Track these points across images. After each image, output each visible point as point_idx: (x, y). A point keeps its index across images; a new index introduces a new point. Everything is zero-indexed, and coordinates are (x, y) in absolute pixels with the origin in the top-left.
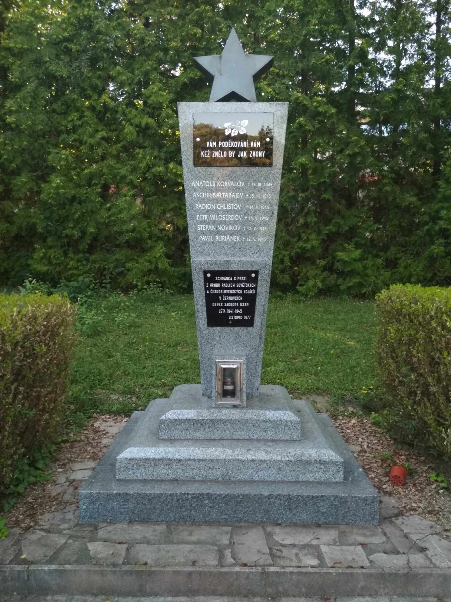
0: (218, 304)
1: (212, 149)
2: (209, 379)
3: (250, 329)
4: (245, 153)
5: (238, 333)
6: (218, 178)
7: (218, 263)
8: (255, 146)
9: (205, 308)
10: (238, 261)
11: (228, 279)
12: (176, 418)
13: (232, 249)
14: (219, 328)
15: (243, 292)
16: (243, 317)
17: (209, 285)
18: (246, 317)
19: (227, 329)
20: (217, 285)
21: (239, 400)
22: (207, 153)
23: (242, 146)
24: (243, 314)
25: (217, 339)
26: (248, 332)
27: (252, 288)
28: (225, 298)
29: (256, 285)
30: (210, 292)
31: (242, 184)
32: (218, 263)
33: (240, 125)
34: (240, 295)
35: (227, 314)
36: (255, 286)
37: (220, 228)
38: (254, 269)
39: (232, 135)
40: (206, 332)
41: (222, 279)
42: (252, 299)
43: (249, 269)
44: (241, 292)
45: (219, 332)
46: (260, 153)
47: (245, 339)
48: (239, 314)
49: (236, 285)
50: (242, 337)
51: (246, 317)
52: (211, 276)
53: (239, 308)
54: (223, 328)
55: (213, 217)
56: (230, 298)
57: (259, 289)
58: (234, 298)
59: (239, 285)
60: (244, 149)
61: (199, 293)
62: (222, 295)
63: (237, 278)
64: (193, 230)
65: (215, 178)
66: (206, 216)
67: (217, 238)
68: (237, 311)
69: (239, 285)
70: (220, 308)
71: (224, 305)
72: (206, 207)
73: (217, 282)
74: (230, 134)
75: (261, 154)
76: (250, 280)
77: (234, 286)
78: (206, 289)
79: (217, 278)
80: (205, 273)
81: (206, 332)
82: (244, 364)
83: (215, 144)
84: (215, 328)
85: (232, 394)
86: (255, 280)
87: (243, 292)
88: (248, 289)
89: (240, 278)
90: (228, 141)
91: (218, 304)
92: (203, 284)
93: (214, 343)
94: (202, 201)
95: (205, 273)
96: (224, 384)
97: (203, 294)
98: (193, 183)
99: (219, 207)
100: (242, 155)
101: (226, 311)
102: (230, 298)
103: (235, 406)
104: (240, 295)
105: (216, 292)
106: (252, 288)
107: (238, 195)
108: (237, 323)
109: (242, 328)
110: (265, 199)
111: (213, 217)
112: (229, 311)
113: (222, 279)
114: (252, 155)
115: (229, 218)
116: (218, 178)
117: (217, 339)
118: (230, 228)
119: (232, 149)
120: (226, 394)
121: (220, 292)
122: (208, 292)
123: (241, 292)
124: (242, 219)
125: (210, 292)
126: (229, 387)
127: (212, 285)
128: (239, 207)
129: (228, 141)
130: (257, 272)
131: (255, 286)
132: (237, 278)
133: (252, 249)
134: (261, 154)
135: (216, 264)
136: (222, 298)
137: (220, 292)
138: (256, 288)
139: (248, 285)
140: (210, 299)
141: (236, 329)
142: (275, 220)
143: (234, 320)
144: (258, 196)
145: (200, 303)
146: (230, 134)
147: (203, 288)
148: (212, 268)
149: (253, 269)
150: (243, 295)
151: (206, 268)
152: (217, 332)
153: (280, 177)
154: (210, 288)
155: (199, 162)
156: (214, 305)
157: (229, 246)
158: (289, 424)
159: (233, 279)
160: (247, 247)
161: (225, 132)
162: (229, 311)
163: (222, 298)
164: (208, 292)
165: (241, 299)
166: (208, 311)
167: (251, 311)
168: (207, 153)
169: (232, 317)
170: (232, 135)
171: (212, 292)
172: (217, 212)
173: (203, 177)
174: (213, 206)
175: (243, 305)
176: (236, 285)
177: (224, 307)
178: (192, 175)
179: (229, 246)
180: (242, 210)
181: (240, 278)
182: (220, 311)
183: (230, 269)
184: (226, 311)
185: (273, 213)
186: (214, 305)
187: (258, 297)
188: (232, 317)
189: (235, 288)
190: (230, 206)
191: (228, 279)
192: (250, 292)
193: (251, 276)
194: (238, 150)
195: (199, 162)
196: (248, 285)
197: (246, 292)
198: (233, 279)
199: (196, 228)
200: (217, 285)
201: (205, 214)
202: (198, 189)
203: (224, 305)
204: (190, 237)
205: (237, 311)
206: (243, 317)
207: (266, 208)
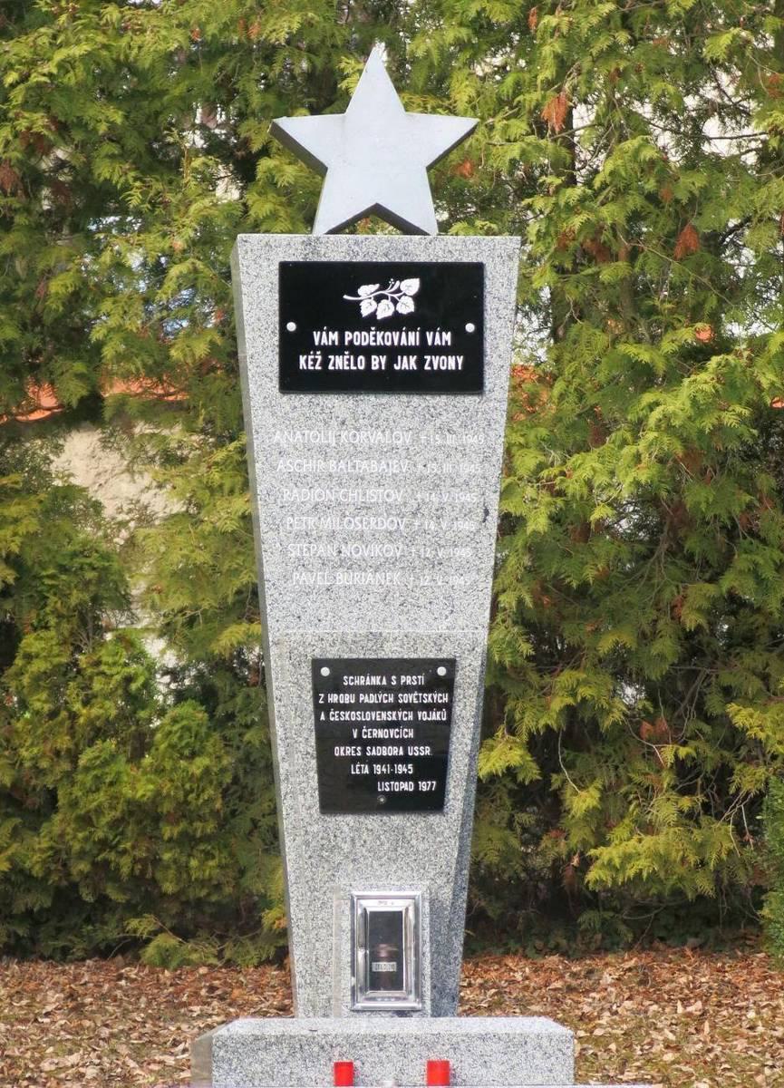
0: (350, 751)
1: (328, 351)
2: (322, 963)
3: (434, 819)
4: (413, 359)
5: (401, 831)
6: (343, 423)
7: (349, 639)
8: (437, 342)
9: (314, 763)
10: (402, 636)
11: (375, 680)
12: (257, 1033)
13: (381, 605)
14: (350, 819)
15: (416, 716)
16: (417, 786)
17: (326, 699)
18: (424, 786)
19: (373, 822)
20: (348, 699)
21: (412, 997)
22: (315, 361)
23: (403, 342)
24: (415, 778)
25: (346, 847)
26: (430, 828)
27: (439, 707)
28: (368, 734)
29: (451, 700)
30: (327, 716)
31: (407, 438)
32: (349, 639)
33: (398, 291)
34: (408, 725)
35: (373, 779)
36: (446, 699)
37: (347, 551)
38: (444, 656)
39: (380, 316)
40: (315, 828)
41: (360, 681)
42: (438, 735)
43: (432, 656)
44: (411, 717)
45: (351, 829)
46: (452, 360)
47: (421, 847)
48: (405, 777)
49: (396, 698)
50: (414, 842)
51: (424, 786)
52: (330, 677)
53: (405, 759)
54: (362, 818)
55: (329, 523)
56: (380, 734)
57: (457, 709)
58: (393, 733)
59: (406, 698)
60: (407, 351)
61: (299, 720)
62: (359, 725)
63: (398, 680)
64: (277, 557)
65: (334, 423)
66: (312, 521)
67: (342, 578)
68: (401, 769)
69: (406, 698)
70: (354, 760)
71: (364, 751)
72: (313, 496)
73: (350, 690)
74: (374, 315)
75: (452, 363)
76: (435, 684)
77: (391, 699)
78: (318, 708)
79: (348, 681)
80: (317, 664)
81: (315, 828)
82: (424, 899)
83: (334, 336)
84: (340, 818)
85: (394, 981)
86: (447, 685)
87: (416, 716)
88: (429, 708)
89: (407, 680)
90: (369, 331)
91: (350, 751)
92: (308, 697)
93: (338, 859)
94: (298, 480)
95: (317, 664)
96: (374, 957)
97: (311, 723)
98: (277, 437)
99: (345, 496)
100: (405, 366)
101: (371, 769)
102: (380, 734)
103: (402, 1013)
104: (408, 725)
105: (346, 716)
106: (439, 707)
107: (395, 466)
108: (400, 804)
109: (414, 817)
110: (465, 477)
111: (329, 523)
112: (378, 769)
113: (360, 681)
114: (431, 364)
115: (373, 523)
116: (343, 423)
117: (346, 847)
118: (375, 550)
119: (379, 350)
120: (376, 981)
121: (354, 716)
122: (323, 717)
123: (411, 717)
124: (407, 526)
125: (327, 716)
126: (385, 967)
127: (333, 698)
128: (396, 497)
129: (369, 331)
130: (451, 664)
131: (446, 699)
132: (398, 680)
133: (434, 607)
134: (452, 363)
135: (344, 642)
136: (360, 733)
137: (354, 716)
138: (448, 707)
139: (428, 698)
140: (328, 736)
141: (397, 820)
142: (494, 531)
143: (391, 795)
144: (447, 468)
145: (302, 747)
146: (374, 315)
147: (311, 707)
148: (332, 653)
149: (441, 656)
150: (416, 724)
151: (318, 654)
152: (346, 829)
153: (503, 420)
154: (327, 707)
155: (292, 380)
156: (340, 751)
157: (372, 600)
158: (545, 1042)
159: (389, 680)
160: (421, 602)
161: (359, 308)
162: (378, 769)
163: (360, 733)
164: (323, 717)
165: (411, 735)
166: (322, 771)
167: (436, 767)
168: (315, 361)
169: (385, 787)
170: (380, 316)
171: (334, 716)
172: (339, 508)
173: (302, 419)
174: (329, 496)
175: (415, 751)
176: (396, 698)
177: (364, 759)
178: (273, 414)
179: (372, 600)
180: (405, 504)
181: (407, 680)
182: (355, 771)
183: (382, 655)
184: (371, 769)
185: (487, 512)
186: (340, 751)
187: (455, 731)
188: (385, 787)
189: (396, 706)
190: (375, 495)
191: (375, 680)
192: (435, 716)
193: (438, 677)
194: (393, 353)
195: (292, 380)
196: (428, 698)
197: (423, 715)
198: (389, 680)
199: (284, 552)
200: (348, 699)
201: (307, 514)
202: (291, 450)
203: (364, 751)
204: (267, 576)
205: (401, 769)
206: (417, 786)
207: (471, 498)
